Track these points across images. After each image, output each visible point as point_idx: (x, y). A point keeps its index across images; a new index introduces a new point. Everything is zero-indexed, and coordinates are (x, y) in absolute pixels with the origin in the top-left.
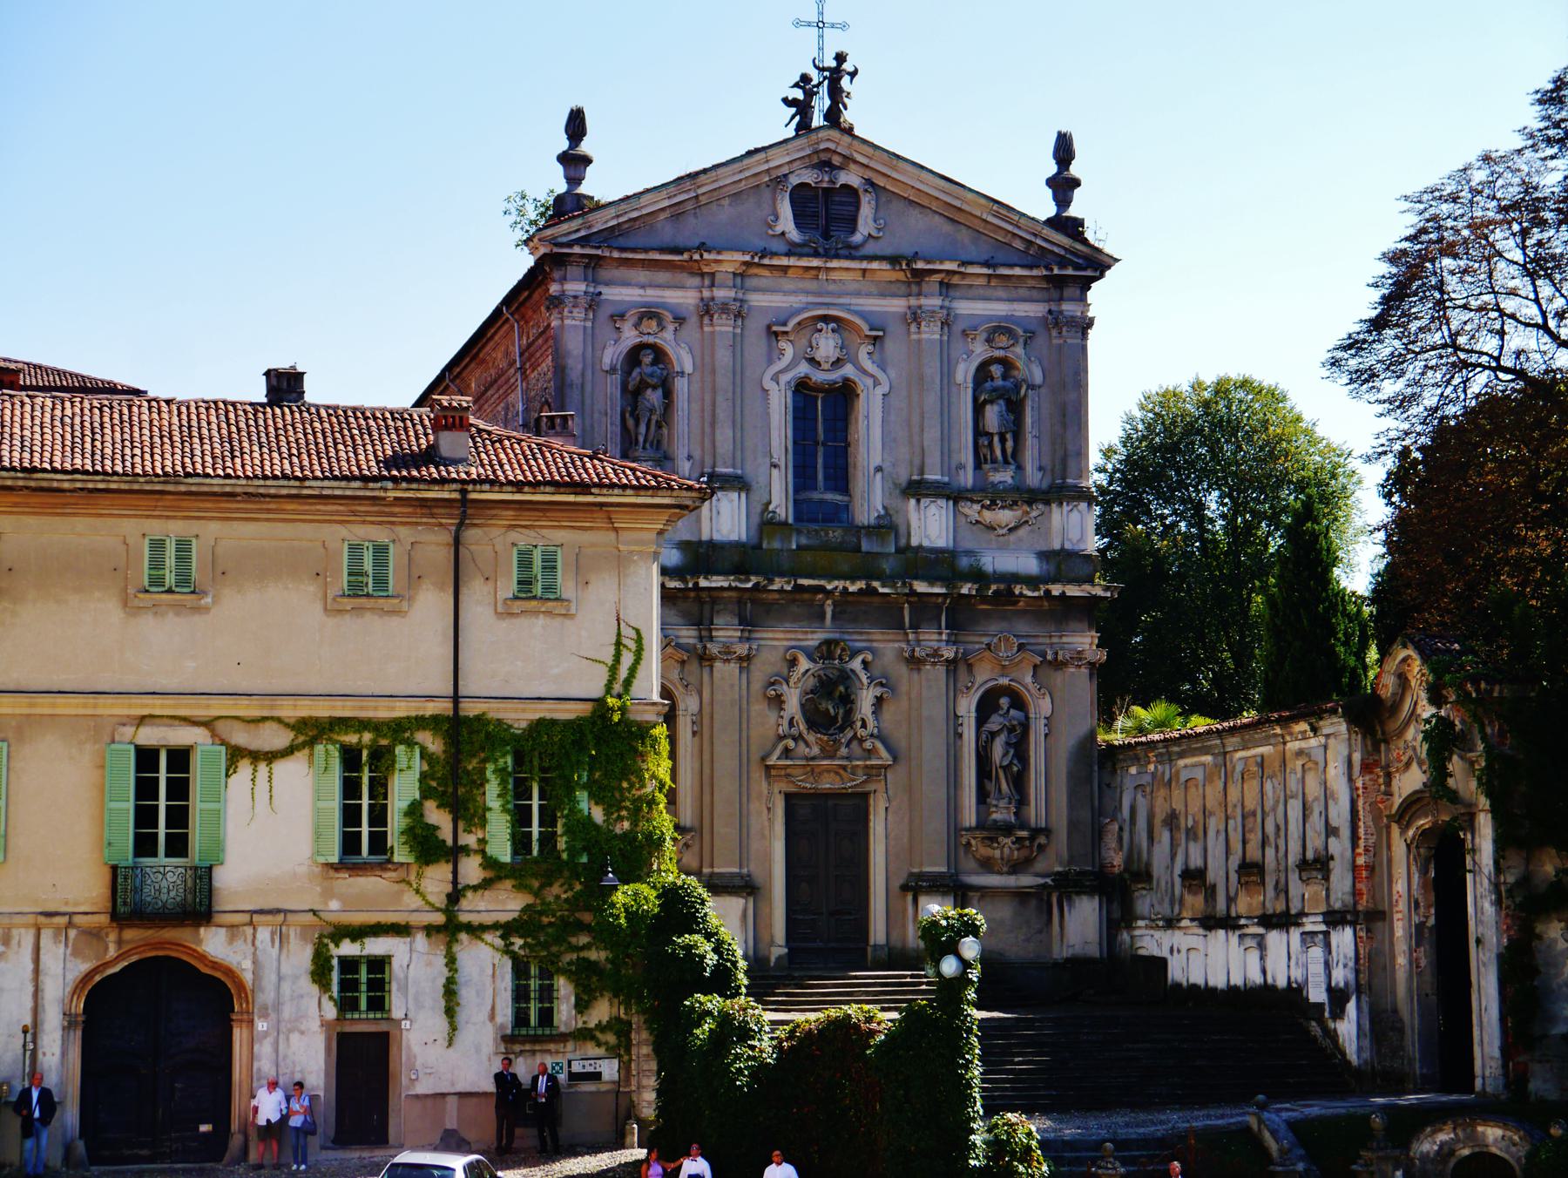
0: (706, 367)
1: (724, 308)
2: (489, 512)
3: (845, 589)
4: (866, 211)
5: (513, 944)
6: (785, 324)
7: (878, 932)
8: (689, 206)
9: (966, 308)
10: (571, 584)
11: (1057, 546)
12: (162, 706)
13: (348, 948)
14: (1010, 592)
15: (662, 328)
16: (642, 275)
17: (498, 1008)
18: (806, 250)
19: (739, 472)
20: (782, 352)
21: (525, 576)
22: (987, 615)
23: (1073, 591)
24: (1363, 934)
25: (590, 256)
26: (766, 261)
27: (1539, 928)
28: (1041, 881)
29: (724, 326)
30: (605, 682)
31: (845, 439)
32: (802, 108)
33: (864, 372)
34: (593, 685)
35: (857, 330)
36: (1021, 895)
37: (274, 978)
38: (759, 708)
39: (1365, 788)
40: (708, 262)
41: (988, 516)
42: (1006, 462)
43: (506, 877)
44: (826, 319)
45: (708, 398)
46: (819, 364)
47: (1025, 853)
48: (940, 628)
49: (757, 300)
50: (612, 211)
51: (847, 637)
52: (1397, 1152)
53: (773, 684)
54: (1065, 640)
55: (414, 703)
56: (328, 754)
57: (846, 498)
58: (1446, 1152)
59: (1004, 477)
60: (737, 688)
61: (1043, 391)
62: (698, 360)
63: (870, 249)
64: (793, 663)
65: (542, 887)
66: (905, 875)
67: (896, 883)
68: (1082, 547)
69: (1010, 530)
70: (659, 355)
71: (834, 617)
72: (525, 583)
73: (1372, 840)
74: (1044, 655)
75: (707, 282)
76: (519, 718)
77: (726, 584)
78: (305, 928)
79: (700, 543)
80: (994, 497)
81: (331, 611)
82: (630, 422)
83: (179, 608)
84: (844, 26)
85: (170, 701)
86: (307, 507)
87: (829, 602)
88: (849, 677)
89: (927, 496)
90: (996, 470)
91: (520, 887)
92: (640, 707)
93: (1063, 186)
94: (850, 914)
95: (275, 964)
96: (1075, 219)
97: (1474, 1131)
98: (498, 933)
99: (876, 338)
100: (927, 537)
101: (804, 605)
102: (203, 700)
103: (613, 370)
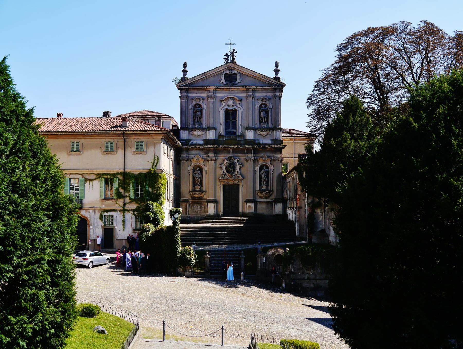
0: (208, 107)
1: (211, 96)
3: (233, 147)
4: (238, 77)
6: (223, 99)
7: (240, 210)
8: (205, 78)
9: (257, 94)
11: (275, 138)
13: (106, 214)
15: (200, 100)
16: (197, 91)
18: (227, 85)
22: (261, 151)
23: (276, 146)
24: (298, 211)
26: (219, 88)
28: (271, 200)
29: (211, 100)
32: (227, 59)
33: (238, 107)
34: (149, 166)
35: (237, 100)
36: (267, 203)
37: (93, 219)
38: (218, 169)
41: (261, 133)
42: (265, 123)
43: (134, 201)
44: (231, 98)
47: (268, 195)
48: (252, 154)
49: (218, 95)
50: (190, 80)
52: (264, 254)
55: (117, 170)
56: (102, 179)
58: (273, 254)
59: (264, 126)
61: (272, 109)
63: (239, 84)
64: (224, 161)
65: (140, 203)
66: (245, 199)
67: (244, 201)
68: (279, 138)
69: (266, 135)
70: (200, 106)
71: (232, 152)
72: (137, 148)
73: (300, 193)
74: (272, 159)
75: (208, 92)
76: (136, 173)
77: (210, 147)
78: (99, 210)
79: (207, 139)
80: (262, 129)
81: (103, 154)
82: (195, 118)
83: (77, 154)
84: (235, 44)
85: (75, 170)
88: (234, 163)
89: (249, 130)
90: (263, 124)
91: (136, 203)
93: (277, 71)
95: (93, 216)
96: (279, 77)
97: (278, 250)
98: (132, 211)
99: (240, 101)
100: (249, 137)
101: (226, 150)
102: (80, 170)
103: (191, 109)
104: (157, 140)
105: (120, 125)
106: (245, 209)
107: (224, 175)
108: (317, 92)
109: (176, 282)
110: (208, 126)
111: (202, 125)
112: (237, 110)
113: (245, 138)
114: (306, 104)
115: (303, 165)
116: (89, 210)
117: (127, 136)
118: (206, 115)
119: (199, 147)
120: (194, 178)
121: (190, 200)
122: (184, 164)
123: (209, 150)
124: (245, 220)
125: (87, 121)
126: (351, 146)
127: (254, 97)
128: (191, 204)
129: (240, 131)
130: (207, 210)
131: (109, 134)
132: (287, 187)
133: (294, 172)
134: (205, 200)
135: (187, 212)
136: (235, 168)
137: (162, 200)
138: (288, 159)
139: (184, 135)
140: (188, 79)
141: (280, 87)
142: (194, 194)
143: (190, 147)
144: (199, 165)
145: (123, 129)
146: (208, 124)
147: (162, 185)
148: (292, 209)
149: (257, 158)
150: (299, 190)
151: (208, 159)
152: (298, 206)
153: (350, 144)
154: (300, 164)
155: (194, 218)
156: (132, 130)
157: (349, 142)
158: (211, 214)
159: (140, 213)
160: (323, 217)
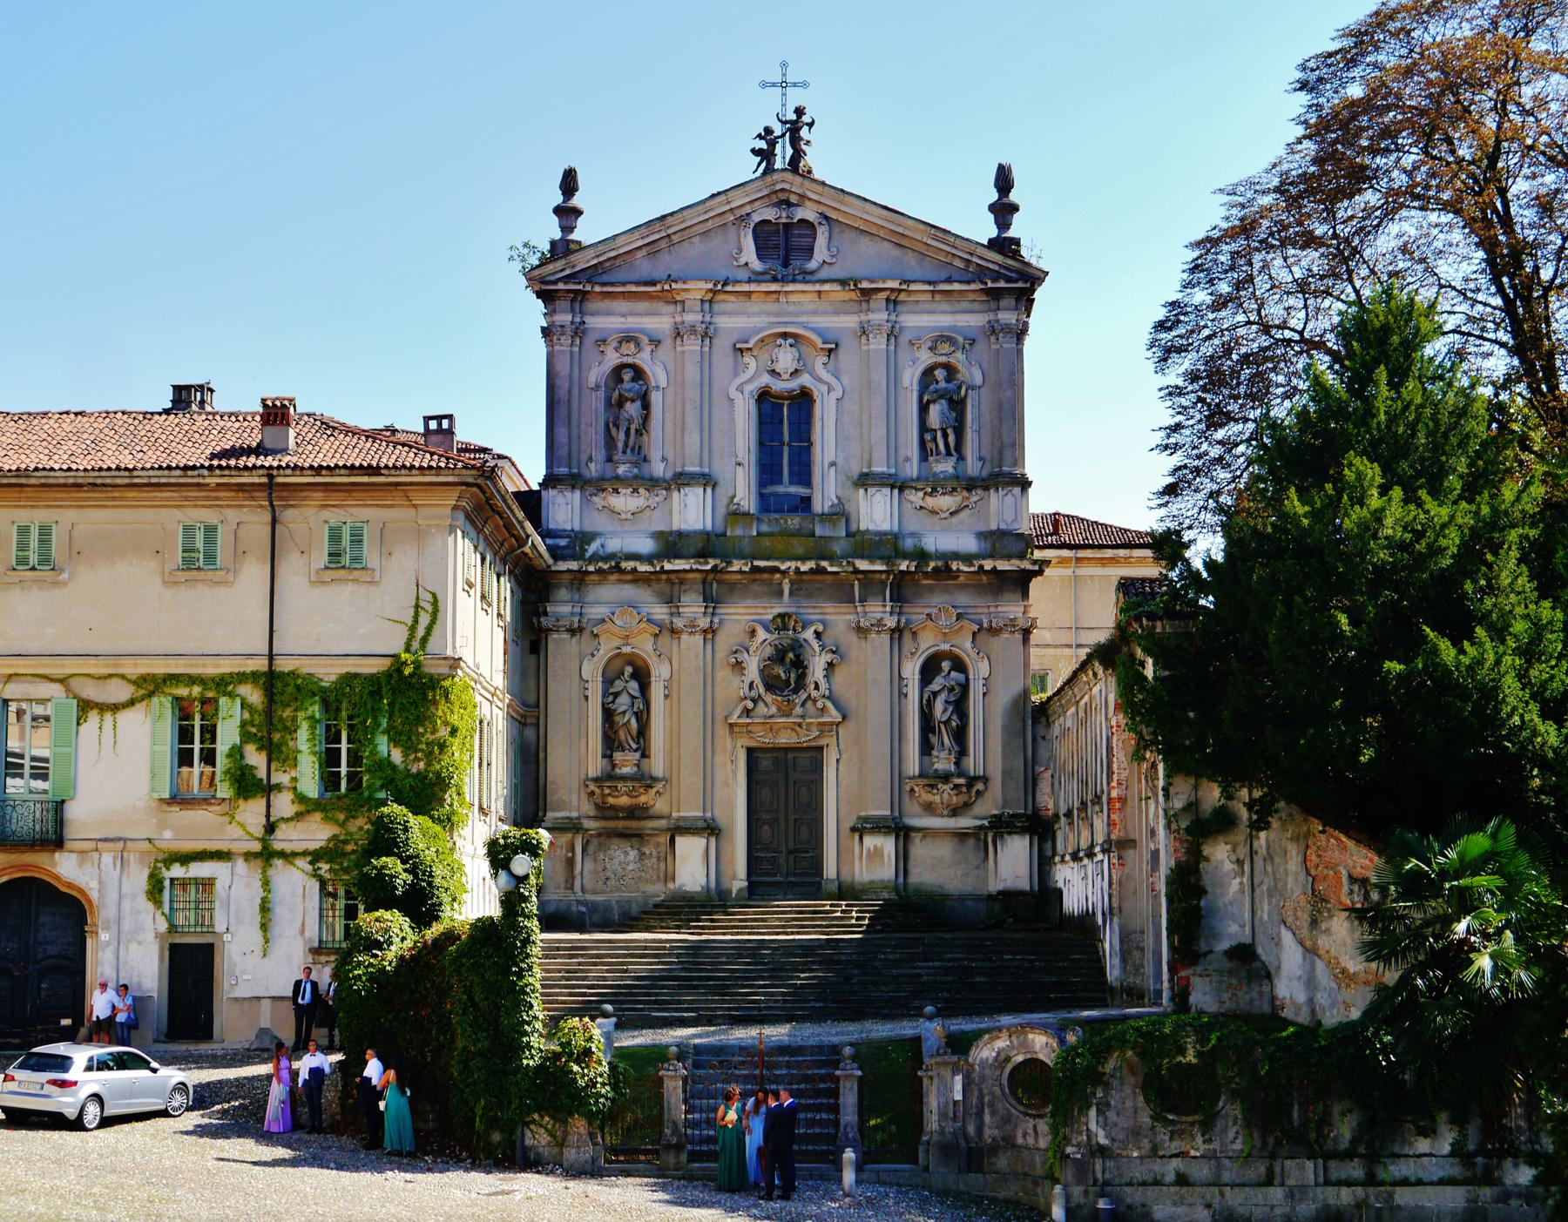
1: (692, 330)
2: (301, 494)
3: (797, 569)
5: (319, 868)
6: (747, 342)
7: (830, 871)
10: (376, 555)
11: (993, 527)
12: (25, 666)
13: (177, 871)
14: (948, 569)
16: (622, 306)
17: (307, 923)
18: (768, 277)
19: (707, 470)
20: (746, 366)
21: (333, 550)
22: (931, 589)
23: (1003, 565)
24: (1115, 861)
25: (576, 292)
26: (729, 288)
27: (1206, 851)
28: (978, 823)
29: (692, 345)
30: (405, 640)
31: (809, 440)
32: (766, 155)
33: (820, 380)
34: (393, 642)
36: (961, 836)
37: (115, 895)
38: (723, 673)
39: (1118, 726)
40: (679, 291)
41: (931, 502)
42: (949, 454)
44: (785, 335)
45: (679, 406)
46: (779, 374)
47: (963, 798)
49: (723, 322)
50: (592, 253)
51: (801, 610)
52: (955, 1058)
53: (736, 652)
54: (1000, 609)
56: (163, 705)
57: (808, 491)
58: (1002, 1060)
59: (945, 467)
60: (701, 657)
61: (982, 390)
62: (672, 376)
63: (823, 274)
64: (753, 633)
67: (847, 825)
70: (639, 374)
71: (791, 594)
72: (335, 555)
73: (1125, 774)
74: (980, 624)
75: (679, 308)
76: (328, 673)
79: (671, 533)
80: (935, 486)
81: (170, 583)
82: (614, 431)
83: (40, 583)
84: (805, 85)
85: (31, 661)
86: (145, 495)
87: (787, 581)
88: (801, 646)
89: (873, 485)
90: (938, 461)
91: (326, 819)
92: (434, 662)
93: (1003, 211)
94: (807, 852)
95: (116, 884)
98: (309, 858)
99: (830, 351)
102: (58, 660)
103: (597, 387)
104: (434, 517)
105: (254, 444)
106: (853, 862)
107: (754, 701)
108: (1201, 296)
109: (518, 1196)
110: (679, 470)
111: (646, 465)
112: (816, 394)
113: (853, 527)
114: (1149, 354)
115: (1141, 626)
116: (95, 855)
117: (285, 494)
118: (669, 415)
119: (634, 570)
120: (608, 714)
121: (587, 824)
122: (561, 648)
123: (682, 582)
124: (854, 914)
125: (95, 425)
126: (1389, 521)
127: (893, 335)
128: (595, 841)
129: (826, 491)
130: (670, 869)
131: (199, 485)
132: (1052, 757)
133: (1095, 675)
134: (663, 823)
135: (573, 878)
136: (806, 667)
137: (451, 805)
138: (1050, 651)
139: (564, 510)
140: (581, 247)
141: (1020, 285)
142: (607, 791)
143: (591, 568)
144: (633, 654)
145: (269, 461)
146: (679, 464)
147: (454, 732)
148: (1081, 859)
149: (908, 622)
150: (1121, 757)
151: (679, 623)
152: (1113, 837)
153: (1378, 515)
154: (1129, 624)
155: (607, 907)
156: (311, 467)
157: (1375, 502)
158: (688, 888)
159: (346, 871)
160: (1241, 883)
